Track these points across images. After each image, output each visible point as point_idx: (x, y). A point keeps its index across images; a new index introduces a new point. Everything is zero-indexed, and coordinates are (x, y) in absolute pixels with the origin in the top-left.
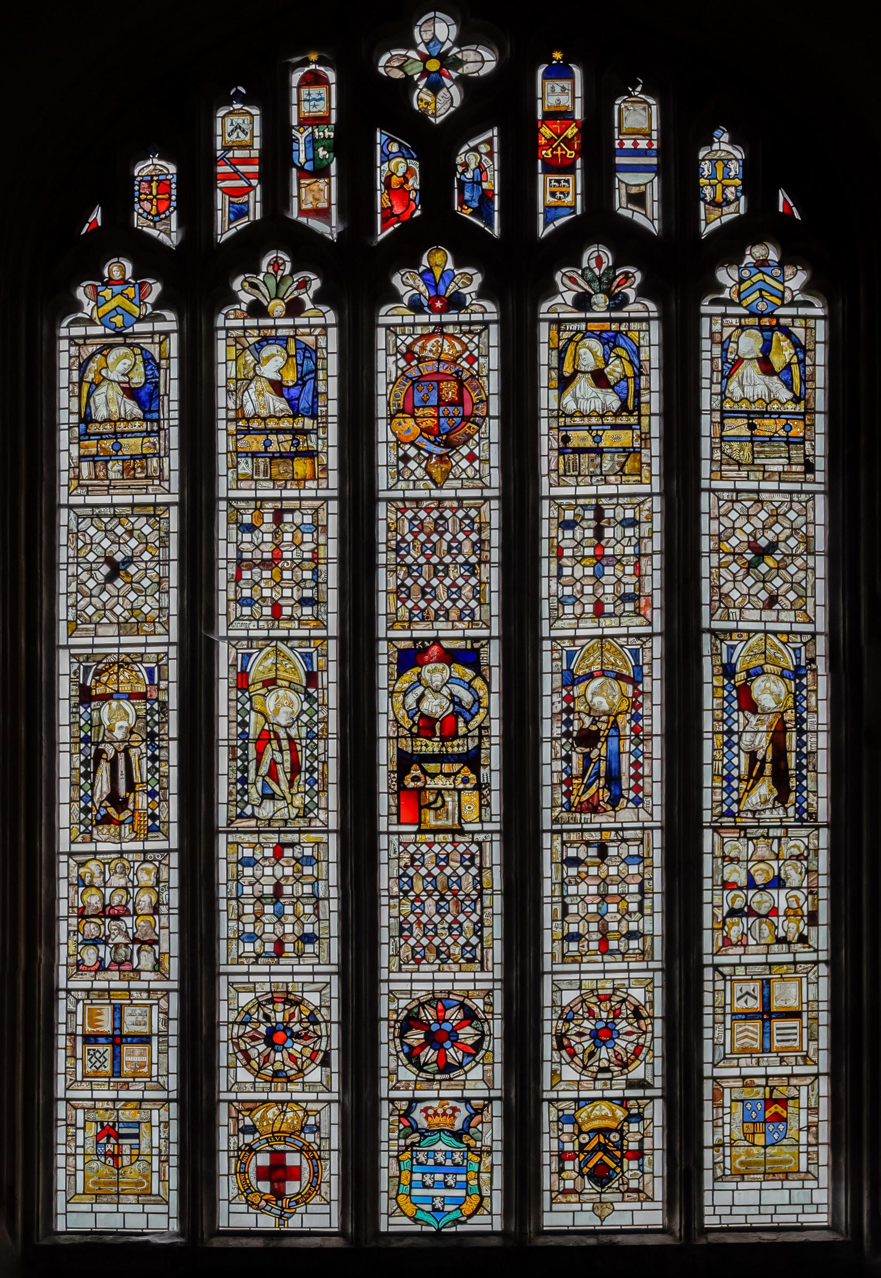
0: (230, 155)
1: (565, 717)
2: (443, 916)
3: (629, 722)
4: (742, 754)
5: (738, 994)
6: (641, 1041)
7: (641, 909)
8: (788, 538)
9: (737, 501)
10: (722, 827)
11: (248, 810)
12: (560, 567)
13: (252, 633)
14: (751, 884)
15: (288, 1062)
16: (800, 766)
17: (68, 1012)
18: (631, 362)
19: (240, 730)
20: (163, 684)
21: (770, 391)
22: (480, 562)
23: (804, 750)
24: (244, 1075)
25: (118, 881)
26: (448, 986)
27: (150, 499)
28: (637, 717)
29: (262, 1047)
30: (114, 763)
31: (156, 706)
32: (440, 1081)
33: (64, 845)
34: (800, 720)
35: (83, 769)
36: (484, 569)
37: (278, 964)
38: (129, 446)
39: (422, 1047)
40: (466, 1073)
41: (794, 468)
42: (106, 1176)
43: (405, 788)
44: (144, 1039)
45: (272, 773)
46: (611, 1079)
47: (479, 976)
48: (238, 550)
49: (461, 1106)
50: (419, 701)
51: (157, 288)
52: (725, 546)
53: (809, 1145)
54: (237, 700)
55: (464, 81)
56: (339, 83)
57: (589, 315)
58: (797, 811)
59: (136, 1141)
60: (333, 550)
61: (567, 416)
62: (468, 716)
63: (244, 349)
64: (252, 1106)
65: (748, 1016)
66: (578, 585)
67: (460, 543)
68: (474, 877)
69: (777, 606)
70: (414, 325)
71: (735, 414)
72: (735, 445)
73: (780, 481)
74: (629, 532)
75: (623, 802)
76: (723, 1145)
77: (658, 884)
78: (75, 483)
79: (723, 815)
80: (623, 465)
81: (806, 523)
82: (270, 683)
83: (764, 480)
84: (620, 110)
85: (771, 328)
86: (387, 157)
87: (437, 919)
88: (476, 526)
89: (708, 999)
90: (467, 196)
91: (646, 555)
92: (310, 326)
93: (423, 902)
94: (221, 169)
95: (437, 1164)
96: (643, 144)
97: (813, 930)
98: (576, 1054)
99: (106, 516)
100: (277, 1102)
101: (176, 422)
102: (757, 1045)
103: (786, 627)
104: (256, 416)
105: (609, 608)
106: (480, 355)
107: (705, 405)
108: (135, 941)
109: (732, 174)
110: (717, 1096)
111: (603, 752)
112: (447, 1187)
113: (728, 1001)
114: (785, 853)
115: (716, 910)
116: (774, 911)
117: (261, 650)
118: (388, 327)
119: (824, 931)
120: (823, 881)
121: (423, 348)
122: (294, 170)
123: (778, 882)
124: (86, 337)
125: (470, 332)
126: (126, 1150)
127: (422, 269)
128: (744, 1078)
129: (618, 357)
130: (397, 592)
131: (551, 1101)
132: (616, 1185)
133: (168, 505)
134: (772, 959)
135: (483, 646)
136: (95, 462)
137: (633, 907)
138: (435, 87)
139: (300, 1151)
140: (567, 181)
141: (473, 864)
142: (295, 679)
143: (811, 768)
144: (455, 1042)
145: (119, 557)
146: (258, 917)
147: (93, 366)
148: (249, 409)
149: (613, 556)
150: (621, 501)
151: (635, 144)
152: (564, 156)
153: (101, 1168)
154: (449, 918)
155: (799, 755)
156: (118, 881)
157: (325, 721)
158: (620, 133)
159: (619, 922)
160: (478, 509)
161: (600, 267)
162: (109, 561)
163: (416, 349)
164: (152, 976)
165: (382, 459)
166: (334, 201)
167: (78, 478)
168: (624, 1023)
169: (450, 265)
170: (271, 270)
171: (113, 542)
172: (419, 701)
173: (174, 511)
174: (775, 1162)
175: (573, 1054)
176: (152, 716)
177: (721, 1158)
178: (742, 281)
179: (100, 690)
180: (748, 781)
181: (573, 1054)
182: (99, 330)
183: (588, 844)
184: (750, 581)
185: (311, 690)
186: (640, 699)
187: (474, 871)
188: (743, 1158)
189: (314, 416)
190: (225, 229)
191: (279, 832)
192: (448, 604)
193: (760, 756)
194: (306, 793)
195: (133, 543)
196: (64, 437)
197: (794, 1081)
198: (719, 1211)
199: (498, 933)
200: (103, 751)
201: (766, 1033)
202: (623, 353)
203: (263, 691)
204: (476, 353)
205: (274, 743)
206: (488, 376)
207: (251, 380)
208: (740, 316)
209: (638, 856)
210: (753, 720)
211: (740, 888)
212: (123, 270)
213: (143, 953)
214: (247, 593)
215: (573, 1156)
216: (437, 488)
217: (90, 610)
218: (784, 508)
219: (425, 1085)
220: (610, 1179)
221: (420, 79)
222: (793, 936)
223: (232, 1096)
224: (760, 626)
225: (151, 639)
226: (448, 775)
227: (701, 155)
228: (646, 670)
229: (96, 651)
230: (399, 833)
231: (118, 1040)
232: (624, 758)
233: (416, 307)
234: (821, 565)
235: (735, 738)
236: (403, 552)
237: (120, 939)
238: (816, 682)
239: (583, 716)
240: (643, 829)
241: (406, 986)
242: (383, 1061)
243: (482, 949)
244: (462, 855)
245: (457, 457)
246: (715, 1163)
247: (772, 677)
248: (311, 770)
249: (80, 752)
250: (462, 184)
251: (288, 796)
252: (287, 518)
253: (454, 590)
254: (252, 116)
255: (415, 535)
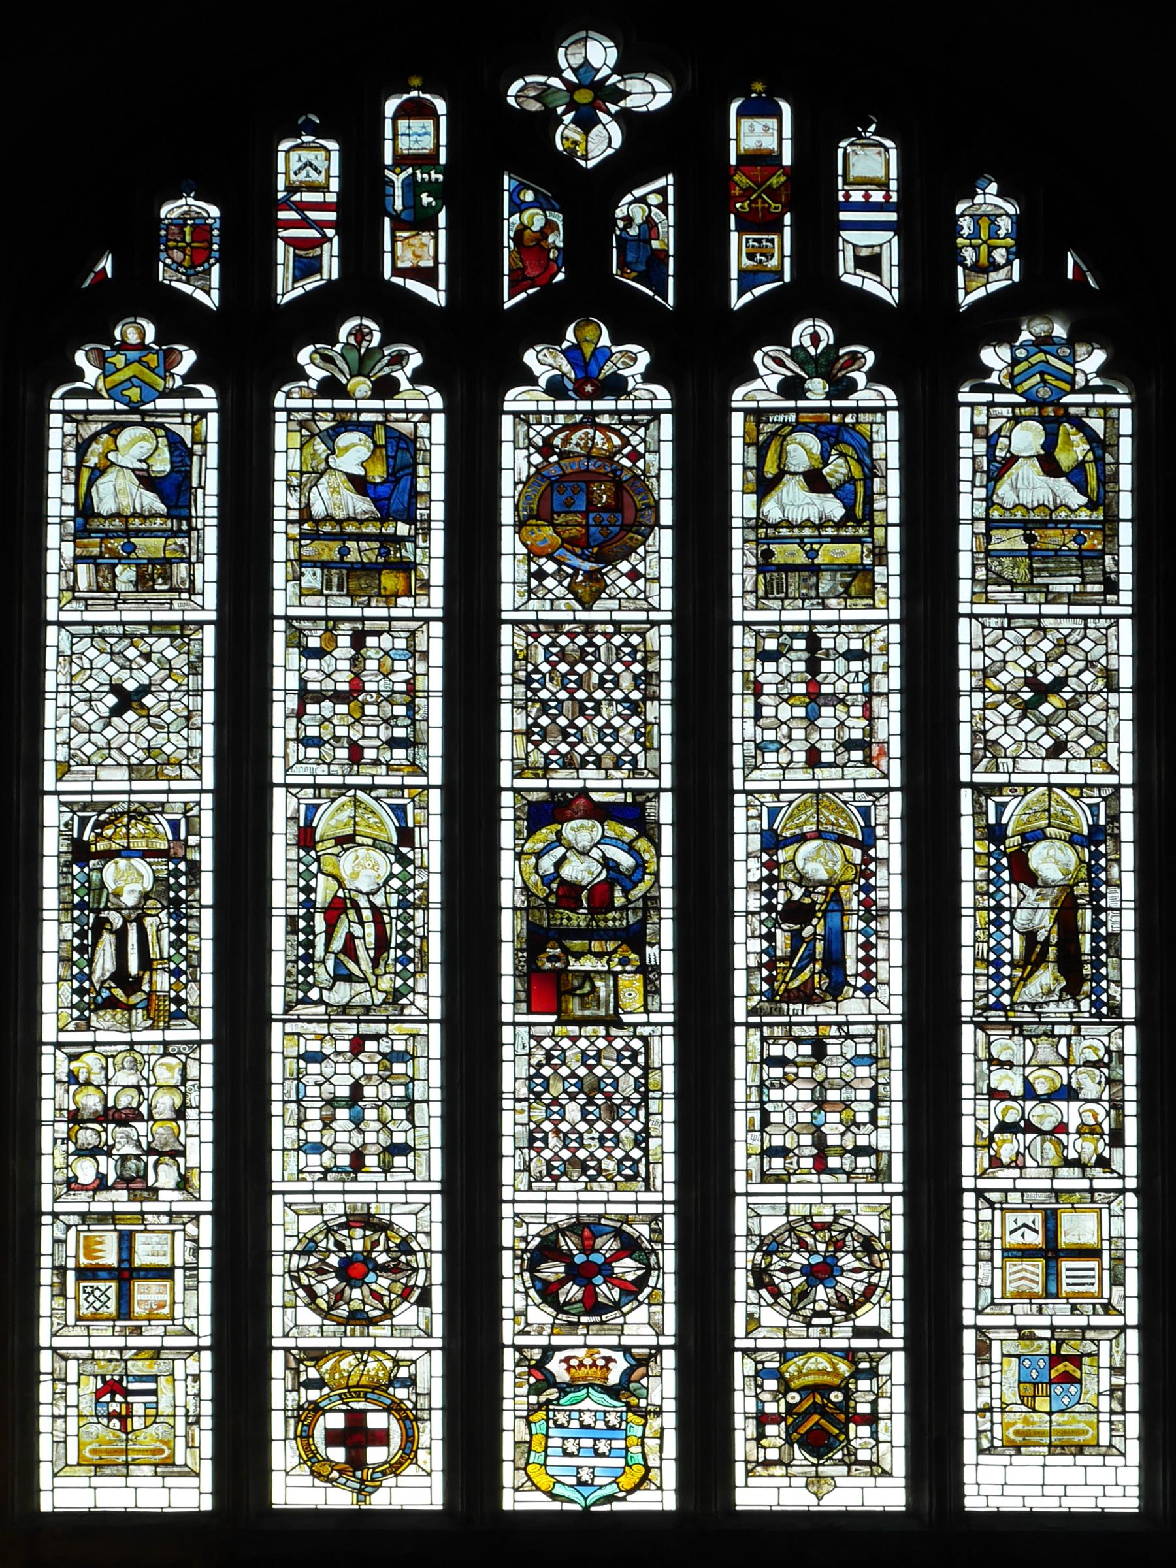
0: (296, 197)
1: (765, 886)
2: (591, 1123)
3: (856, 894)
4: (1016, 935)
5: (1011, 1226)
6: (874, 1279)
7: (874, 1119)
8: (1081, 672)
9: (1010, 628)
10: (988, 1023)
11: (314, 994)
12: (758, 707)
13: (319, 780)
14: (1029, 1092)
15: (370, 1300)
16: (1096, 951)
17: (56, 1241)
18: (860, 461)
19: (302, 897)
20: (193, 840)
21: (1055, 495)
22: (645, 699)
23: (1103, 931)
24: (306, 1316)
25: (126, 1077)
26: (599, 1209)
27: (176, 616)
28: (867, 889)
29: (333, 1282)
30: (121, 936)
31: (182, 866)
32: (587, 1325)
33: (49, 1032)
34: (1096, 896)
35: (76, 942)
36: (651, 708)
37: (355, 1180)
38: (148, 548)
39: (561, 1283)
40: (624, 1315)
41: (1089, 588)
42: (110, 1442)
43: (539, 970)
44: (164, 1273)
45: (349, 948)
46: (831, 1326)
47: (643, 1196)
48: (301, 679)
49: (618, 1356)
50: (559, 864)
51: (189, 357)
52: (993, 683)
53: (1112, 1412)
54: (299, 860)
55: (626, 118)
56: (449, 115)
57: (801, 404)
58: (1092, 1004)
59: (153, 1399)
60: (436, 680)
61: (769, 526)
62: (628, 884)
63: (313, 436)
64: (317, 1355)
65: (1026, 1253)
66: (784, 729)
67: (617, 675)
68: (636, 1080)
69: (1066, 755)
70: (554, 413)
71: (1006, 524)
72: (1007, 561)
73: (1069, 604)
74: (856, 665)
75: (848, 990)
76: (991, 1409)
77: (897, 1090)
78: (68, 595)
79: (987, 1007)
80: (847, 586)
81: (1107, 654)
82: (345, 841)
83: (1047, 602)
84: (845, 155)
85: (1054, 418)
86: (518, 207)
87: (582, 1127)
88: (639, 656)
89: (968, 1231)
90: (630, 257)
91: (879, 694)
92: (407, 411)
93: (563, 1107)
94: (282, 215)
95: (583, 1427)
96: (877, 196)
97: (1117, 1153)
98: (781, 1294)
99: (112, 635)
100: (354, 1350)
101: (215, 522)
102: (1039, 1289)
103: (1080, 779)
104: (329, 518)
105: (827, 757)
106: (647, 450)
107: (965, 512)
108: (150, 1151)
109: (1002, 233)
110: (983, 1350)
111: (820, 930)
112: (597, 1454)
113: (998, 1234)
114: (1078, 1058)
115: (980, 1124)
116: (1062, 1127)
117: (333, 800)
118: (516, 414)
119: (1132, 1155)
120: (1131, 1093)
121: (566, 441)
122: (387, 220)
123: (1068, 1093)
124: (87, 412)
125: (633, 422)
126: (138, 1409)
127: (565, 345)
128: (1019, 1328)
129: (841, 455)
130: (528, 733)
131: (746, 1352)
132: (839, 1455)
133: (201, 624)
134: (1058, 1184)
135: (650, 800)
136: (97, 565)
137: (863, 1117)
138: (587, 122)
139: (388, 1409)
140: (772, 241)
141: (635, 1063)
142: (382, 836)
143: (1112, 952)
144: (610, 1278)
145: (130, 686)
146: (327, 1123)
147: (97, 448)
148: (318, 510)
149: (834, 694)
150: (844, 628)
151: (867, 196)
152: (766, 210)
153: (102, 1432)
154: (601, 1126)
155: (1096, 938)
156: (126, 1077)
157: (425, 887)
158: (845, 183)
159: (843, 1134)
160: (643, 635)
161: (816, 346)
162: (116, 688)
163: (557, 441)
164: (177, 1195)
165: (506, 573)
166: (442, 257)
167: (73, 589)
168: (850, 1257)
169: (605, 340)
170: (352, 340)
171: (122, 667)
172: (559, 864)
173: (209, 632)
174: (1064, 1433)
175: (776, 1293)
176: (177, 878)
177: (988, 1426)
178: (1015, 361)
179: (102, 846)
180: (1024, 968)
181: (776, 1293)
182: (107, 404)
183: (799, 1041)
184: (1027, 724)
185: (404, 850)
186: (872, 866)
187: (636, 1071)
188: (1019, 1426)
189: (411, 520)
190: (288, 289)
191: (358, 1022)
192: (600, 749)
193: (1041, 937)
194: (396, 974)
195: (151, 668)
196: (53, 534)
197: (1090, 1334)
198: (984, 1490)
199: (670, 1143)
200: (107, 920)
201: (1052, 1273)
202: (850, 451)
203: (337, 850)
204: (641, 448)
205: (352, 915)
206: (658, 477)
207: (322, 474)
208: (1013, 406)
209: (870, 1056)
210: (1031, 893)
211: (1015, 1099)
212: (142, 334)
213: (161, 1168)
214: (313, 732)
215: (776, 1419)
216: (585, 609)
217: (89, 749)
218: (1075, 637)
219: (565, 1330)
220: (831, 1448)
221: (565, 113)
222: (1089, 1156)
223: (290, 1343)
224: (1043, 779)
225: (175, 785)
226: (599, 955)
227: (960, 208)
228: (880, 831)
229: (96, 798)
230: (529, 1025)
231: (126, 1275)
232: (850, 939)
233: (556, 389)
234: (1126, 703)
235: (1006, 916)
236: (535, 685)
237: (130, 1150)
238: (1118, 850)
239: (791, 886)
240: (877, 1023)
241: (541, 1208)
242: (507, 1297)
243: (648, 1164)
244: (619, 1052)
245: (613, 575)
246: (979, 1432)
247: (1058, 843)
248: (404, 946)
249: (73, 920)
250: (623, 242)
251: (372, 979)
252: (371, 641)
253: (608, 734)
254: (328, 151)
255: (554, 665)
